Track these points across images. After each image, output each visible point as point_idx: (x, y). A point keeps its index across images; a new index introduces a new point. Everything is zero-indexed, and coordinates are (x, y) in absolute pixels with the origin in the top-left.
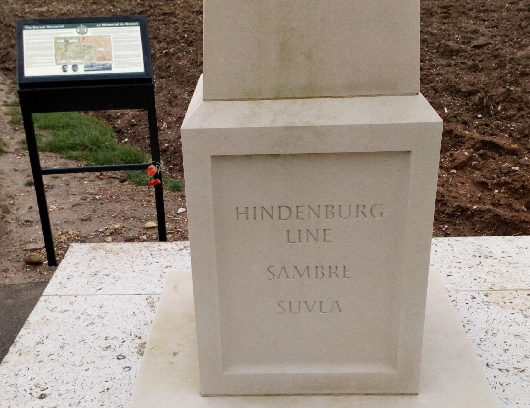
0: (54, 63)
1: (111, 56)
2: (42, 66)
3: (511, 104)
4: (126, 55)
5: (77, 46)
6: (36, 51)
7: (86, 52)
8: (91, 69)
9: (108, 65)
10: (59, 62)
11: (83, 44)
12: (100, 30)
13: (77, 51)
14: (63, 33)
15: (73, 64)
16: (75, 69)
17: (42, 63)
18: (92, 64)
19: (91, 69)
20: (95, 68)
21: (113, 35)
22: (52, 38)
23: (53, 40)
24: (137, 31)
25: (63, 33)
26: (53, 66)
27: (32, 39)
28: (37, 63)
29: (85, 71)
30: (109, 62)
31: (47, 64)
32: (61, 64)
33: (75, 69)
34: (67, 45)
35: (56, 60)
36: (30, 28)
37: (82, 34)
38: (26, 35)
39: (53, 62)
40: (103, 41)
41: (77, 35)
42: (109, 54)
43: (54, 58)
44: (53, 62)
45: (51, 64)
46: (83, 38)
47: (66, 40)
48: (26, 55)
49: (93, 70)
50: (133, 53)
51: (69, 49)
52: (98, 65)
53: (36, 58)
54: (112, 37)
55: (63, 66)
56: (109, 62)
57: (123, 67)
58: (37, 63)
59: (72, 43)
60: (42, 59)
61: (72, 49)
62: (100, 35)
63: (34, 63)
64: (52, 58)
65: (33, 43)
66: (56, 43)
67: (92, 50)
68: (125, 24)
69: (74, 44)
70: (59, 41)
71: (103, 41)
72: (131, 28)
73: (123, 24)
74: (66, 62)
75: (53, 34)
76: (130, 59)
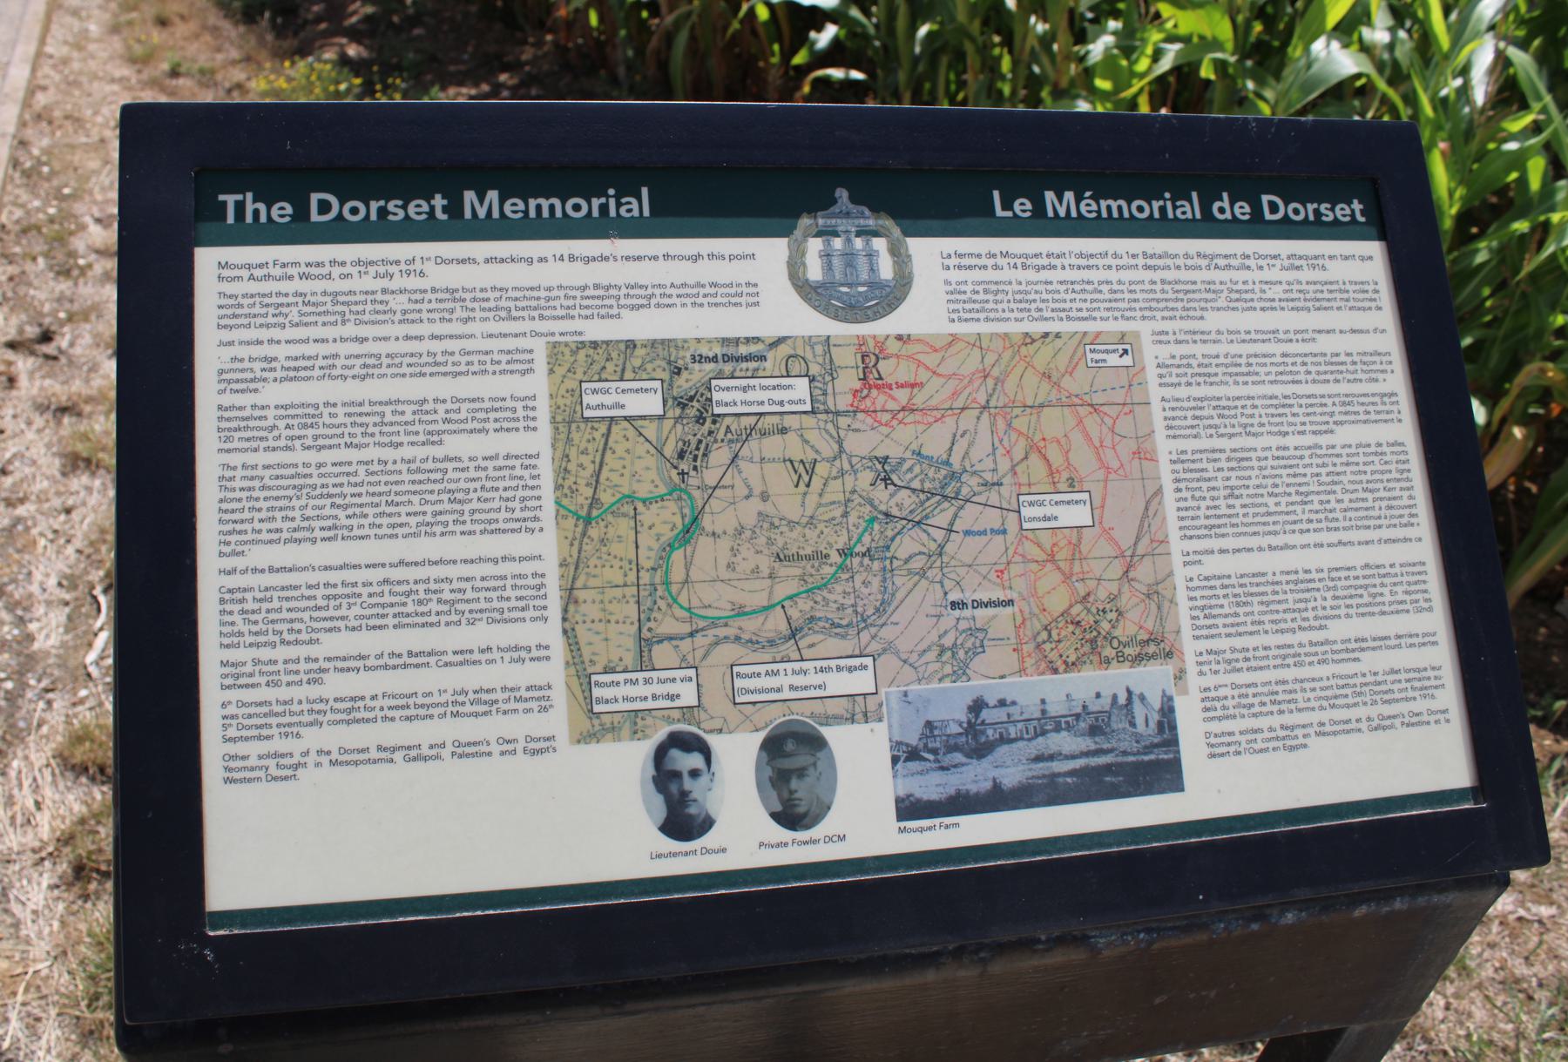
0: (557, 720)
1: (1158, 594)
2: (414, 755)
3: (294, 84)
4: (1301, 581)
5: (803, 472)
6: (334, 532)
7: (907, 545)
8: (974, 776)
9: (1145, 720)
10: (617, 693)
11: (862, 443)
12: (1025, 261)
13: (811, 541)
14: (644, 298)
15: (776, 717)
16: (801, 789)
17: (412, 708)
18: (977, 706)
19: (974, 776)
20: (1010, 769)
21: (1160, 337)
22: (519, 364)
23: (538, 384)
24: (1354, 297)
25: (644, 298)
26: (540, 747)
27: (295, 372)
28: (352, 711)
29: (909, 809)
30: (1150, 679)
31: (467, 729)
32: (635, 722)
33: (801, 789)
34: (691, 455)
35: (582, 675)
36: (282, 211)
37: (853, 311)
38: (232, 312)
39: (539, 697)
40: (1072, 402)
41: (808, 322)
42: (1143, 572)
43: (551, 633)
44: (539, 697)
45: (520, 726)
46: (870, 357)
47: (684, 384)
48: (230, 596)
49: (997, 799)
50: (1355, 557)
51: (719, 518)
52: (1046, 723)
53: (333, 644)
54: (1151, 354)
55: (660, 754)
56: (1150, 679)
57: (1288, 739)
58: (352, 711)
59: (756, 427)
60: (417, 659)
61: (749, 511)
62: (1037, 328)
63: (317, 714)
64: (526, 633)
65: (309, 415)
66: (568, 419)
67: (969, 517)
68: (1039, 209)
69: (772, 446)
70: (598, 400)
71: (1072, 402)
72: (1314, 261)
73: (1242, 210)
74: (688, 696)
75: (535, 302)
76: (1339, 630)
